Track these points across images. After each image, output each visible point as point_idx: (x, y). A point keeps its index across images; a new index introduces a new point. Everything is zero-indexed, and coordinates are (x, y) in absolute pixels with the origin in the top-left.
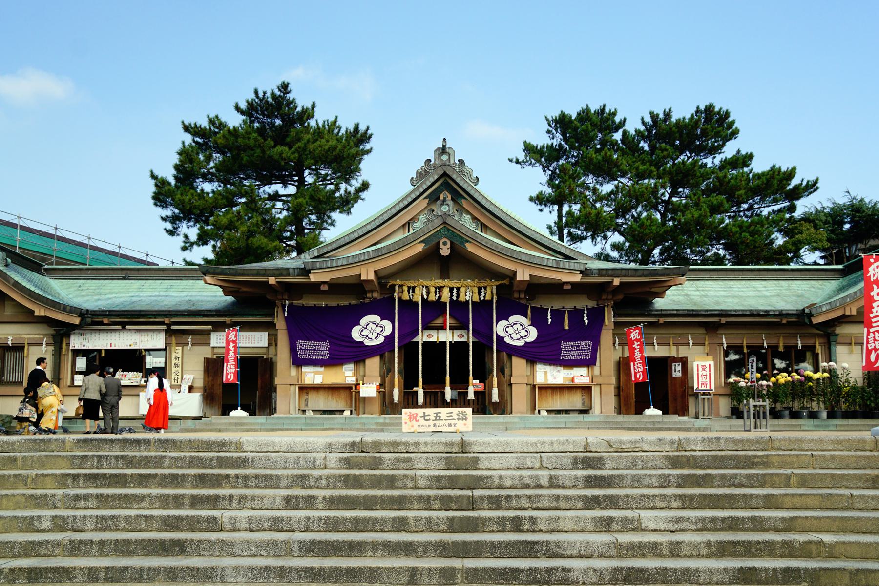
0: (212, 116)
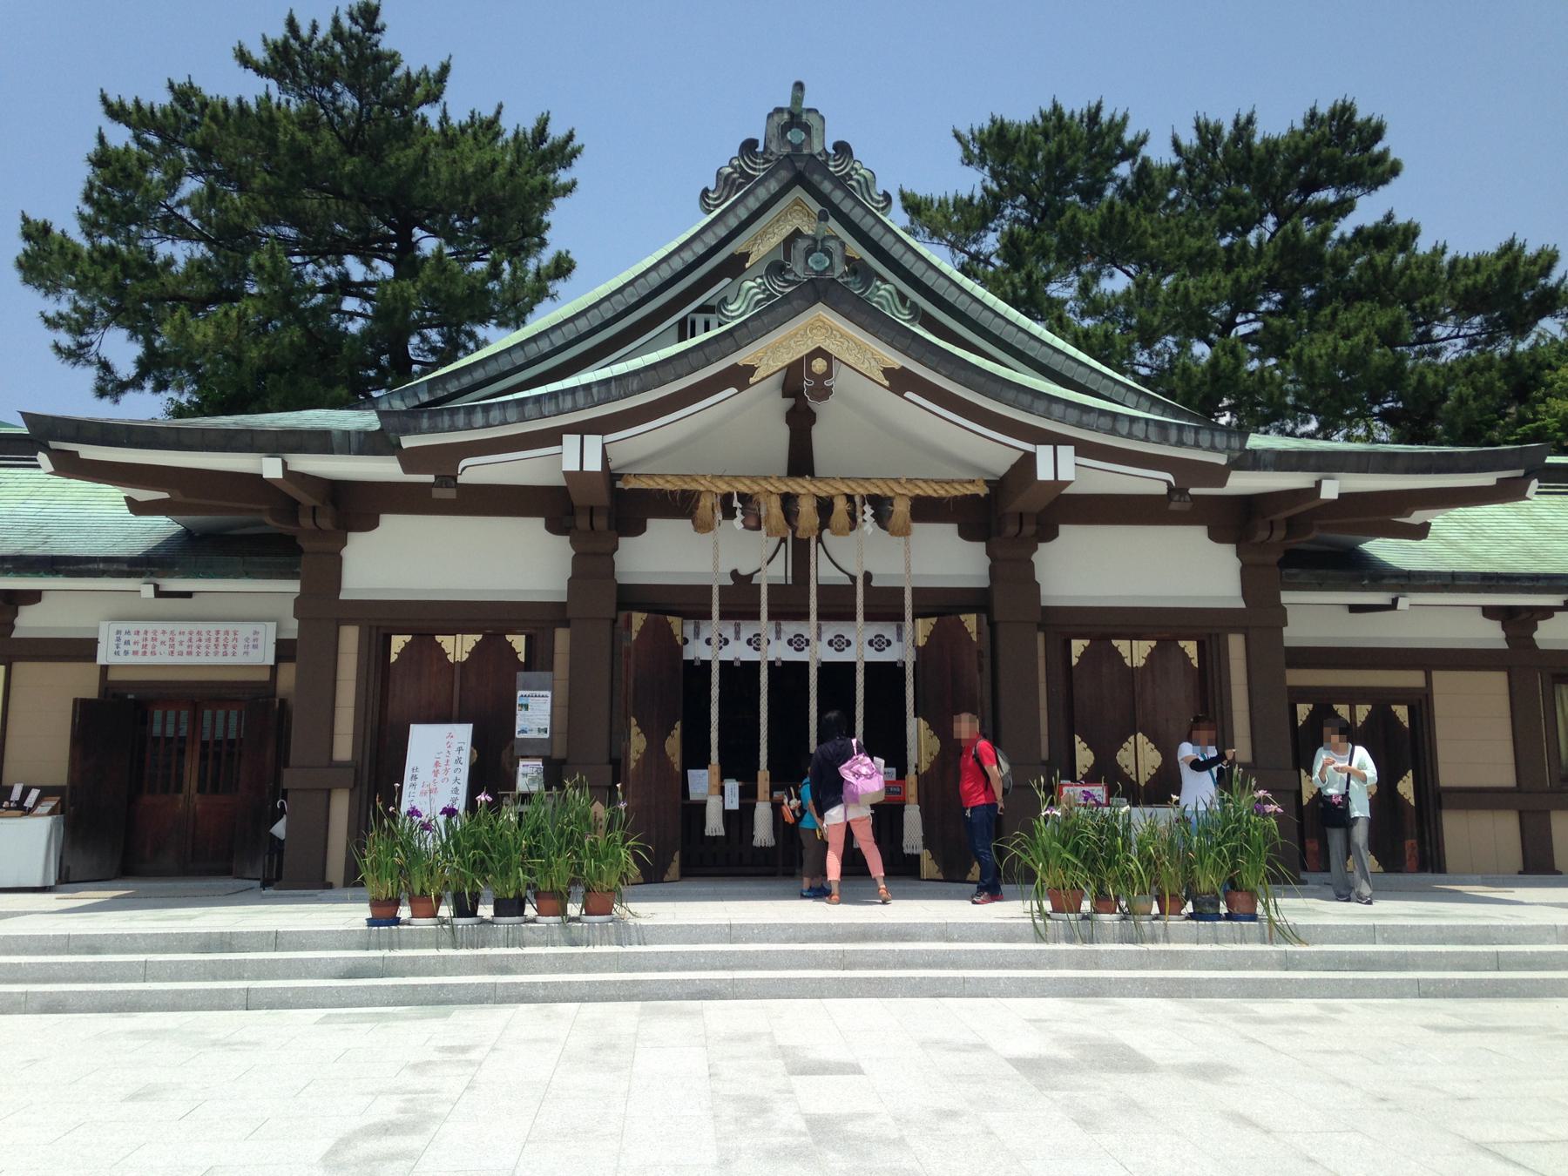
0: (180, 80)
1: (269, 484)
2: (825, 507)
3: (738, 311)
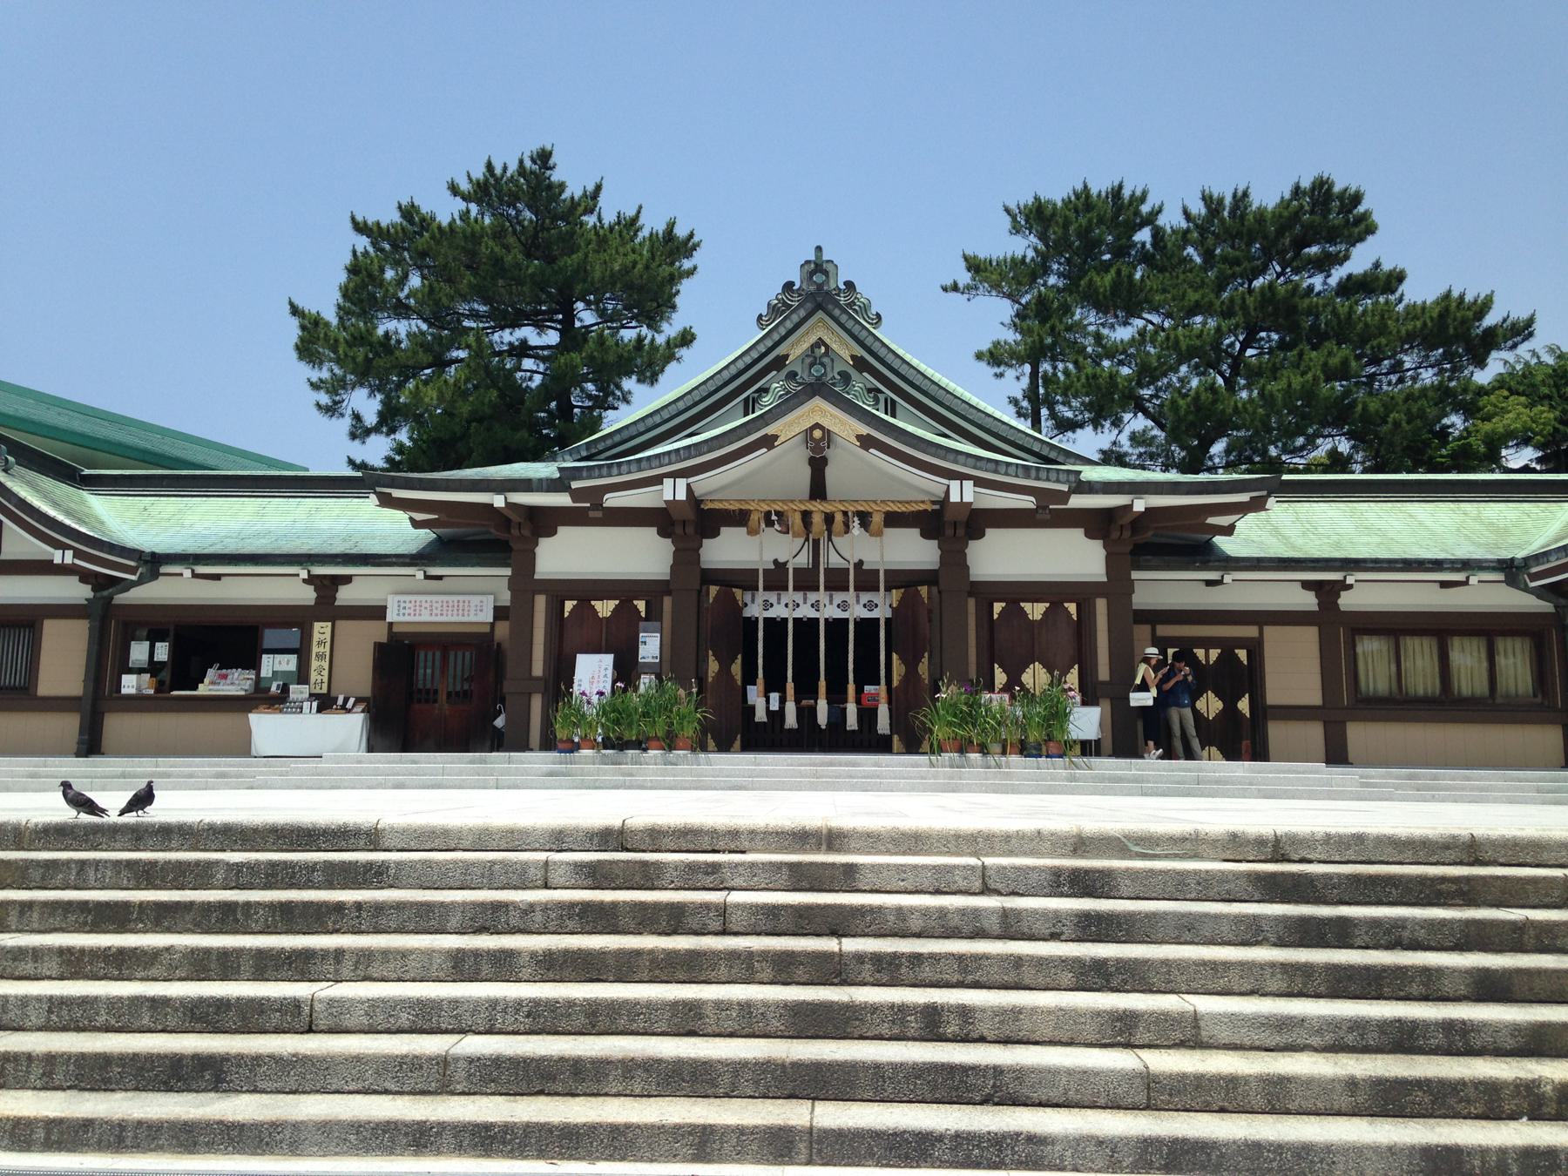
1: (497, 510)
2: (829, 519)
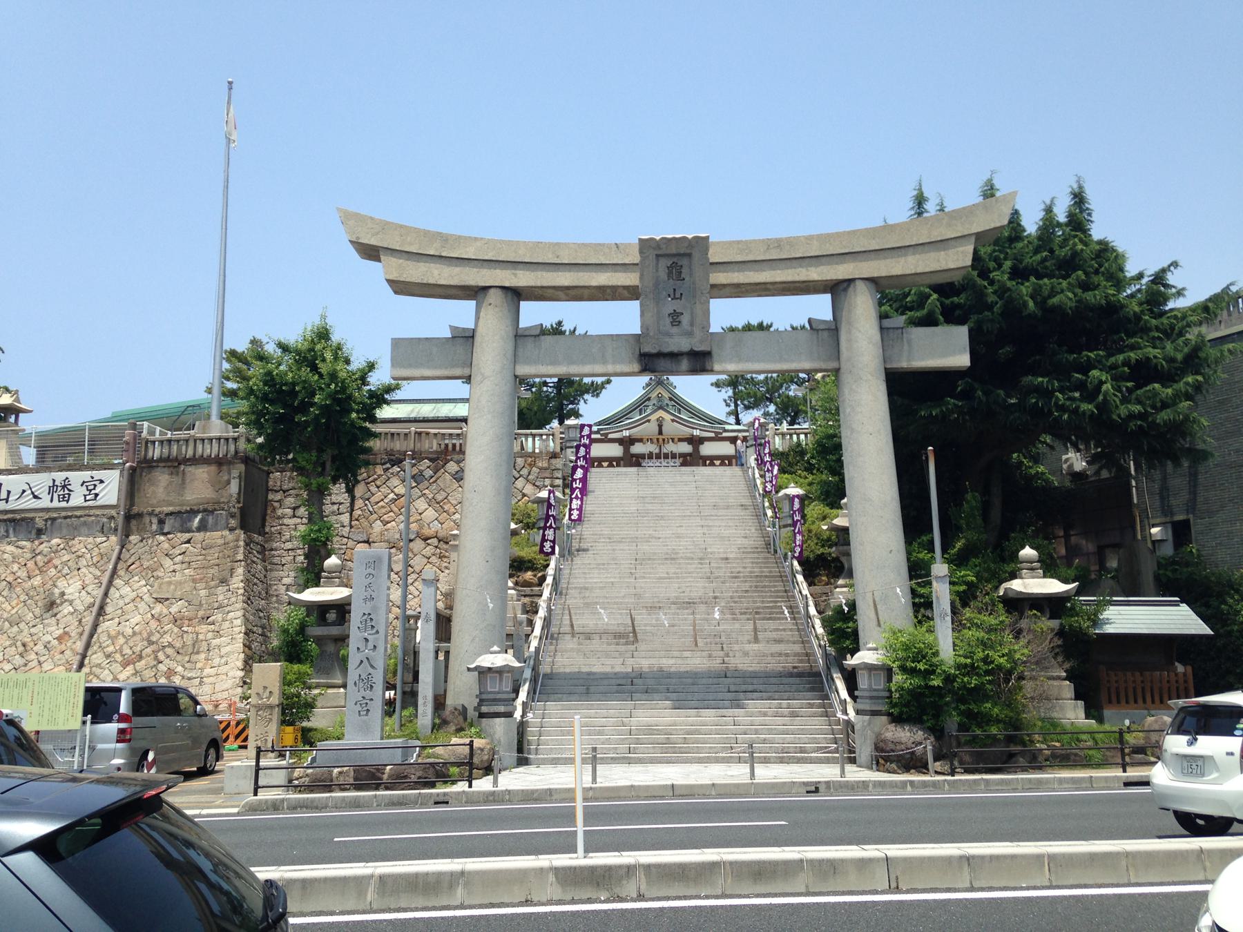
3: (649, 411)
